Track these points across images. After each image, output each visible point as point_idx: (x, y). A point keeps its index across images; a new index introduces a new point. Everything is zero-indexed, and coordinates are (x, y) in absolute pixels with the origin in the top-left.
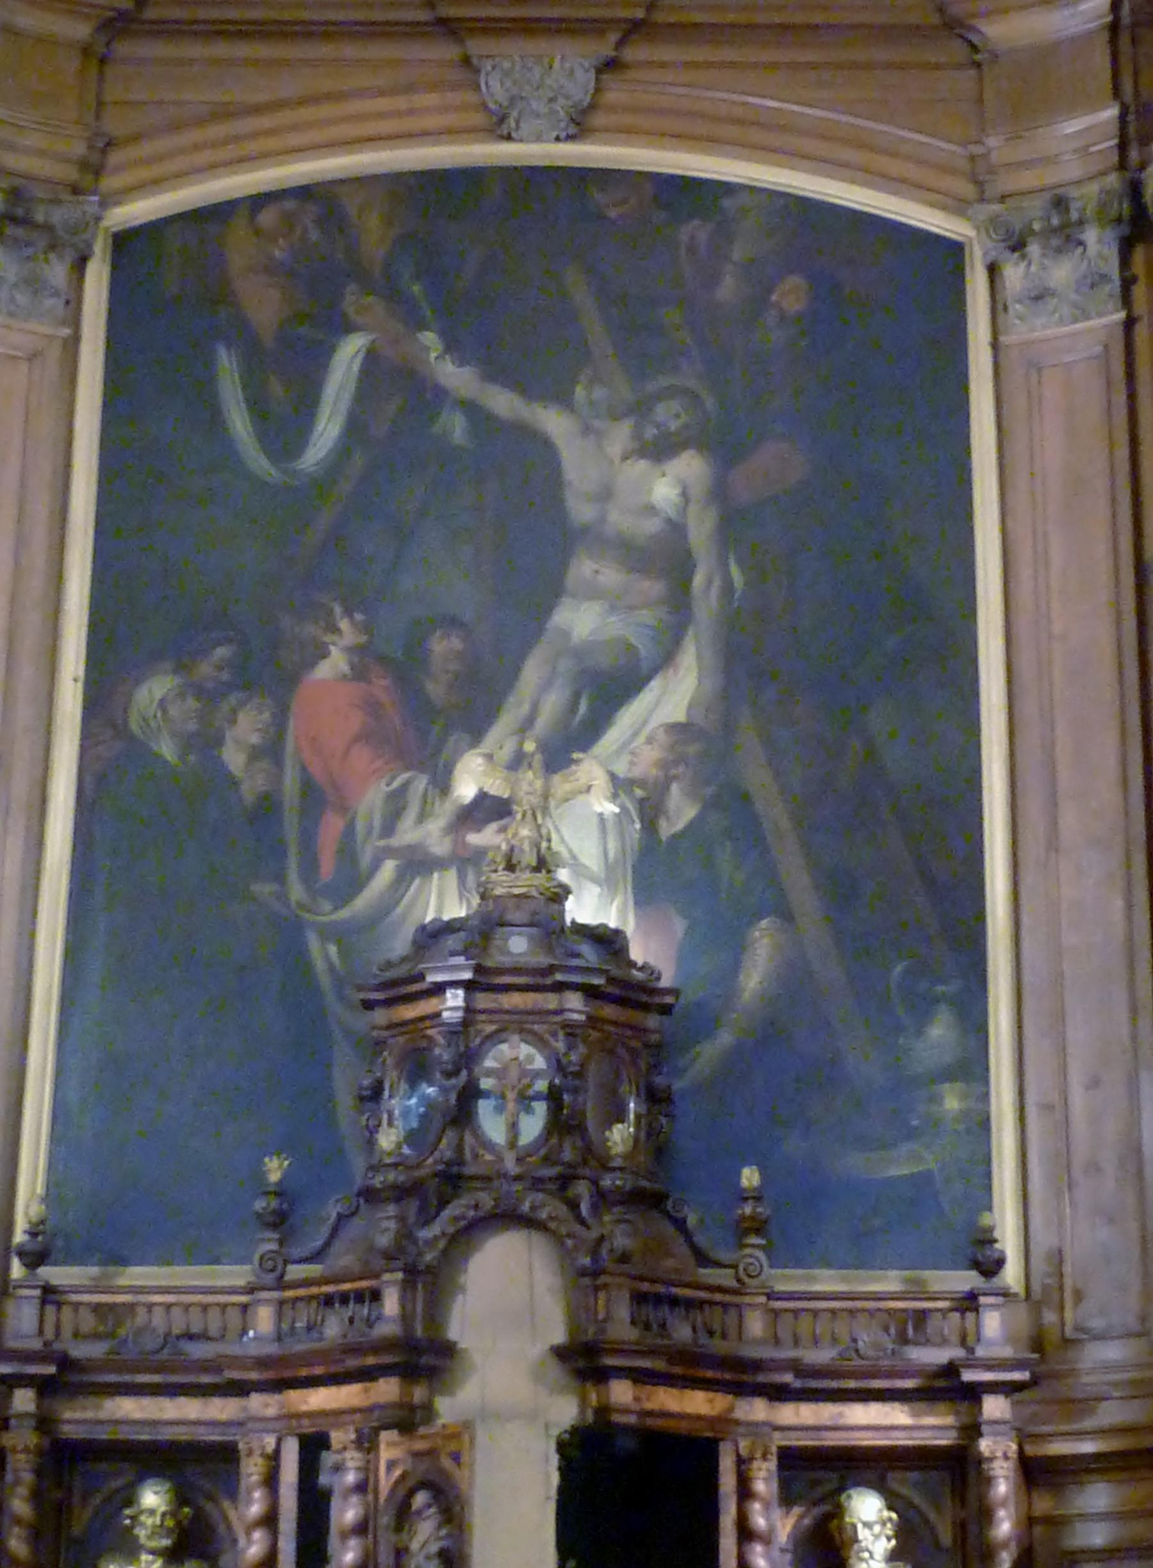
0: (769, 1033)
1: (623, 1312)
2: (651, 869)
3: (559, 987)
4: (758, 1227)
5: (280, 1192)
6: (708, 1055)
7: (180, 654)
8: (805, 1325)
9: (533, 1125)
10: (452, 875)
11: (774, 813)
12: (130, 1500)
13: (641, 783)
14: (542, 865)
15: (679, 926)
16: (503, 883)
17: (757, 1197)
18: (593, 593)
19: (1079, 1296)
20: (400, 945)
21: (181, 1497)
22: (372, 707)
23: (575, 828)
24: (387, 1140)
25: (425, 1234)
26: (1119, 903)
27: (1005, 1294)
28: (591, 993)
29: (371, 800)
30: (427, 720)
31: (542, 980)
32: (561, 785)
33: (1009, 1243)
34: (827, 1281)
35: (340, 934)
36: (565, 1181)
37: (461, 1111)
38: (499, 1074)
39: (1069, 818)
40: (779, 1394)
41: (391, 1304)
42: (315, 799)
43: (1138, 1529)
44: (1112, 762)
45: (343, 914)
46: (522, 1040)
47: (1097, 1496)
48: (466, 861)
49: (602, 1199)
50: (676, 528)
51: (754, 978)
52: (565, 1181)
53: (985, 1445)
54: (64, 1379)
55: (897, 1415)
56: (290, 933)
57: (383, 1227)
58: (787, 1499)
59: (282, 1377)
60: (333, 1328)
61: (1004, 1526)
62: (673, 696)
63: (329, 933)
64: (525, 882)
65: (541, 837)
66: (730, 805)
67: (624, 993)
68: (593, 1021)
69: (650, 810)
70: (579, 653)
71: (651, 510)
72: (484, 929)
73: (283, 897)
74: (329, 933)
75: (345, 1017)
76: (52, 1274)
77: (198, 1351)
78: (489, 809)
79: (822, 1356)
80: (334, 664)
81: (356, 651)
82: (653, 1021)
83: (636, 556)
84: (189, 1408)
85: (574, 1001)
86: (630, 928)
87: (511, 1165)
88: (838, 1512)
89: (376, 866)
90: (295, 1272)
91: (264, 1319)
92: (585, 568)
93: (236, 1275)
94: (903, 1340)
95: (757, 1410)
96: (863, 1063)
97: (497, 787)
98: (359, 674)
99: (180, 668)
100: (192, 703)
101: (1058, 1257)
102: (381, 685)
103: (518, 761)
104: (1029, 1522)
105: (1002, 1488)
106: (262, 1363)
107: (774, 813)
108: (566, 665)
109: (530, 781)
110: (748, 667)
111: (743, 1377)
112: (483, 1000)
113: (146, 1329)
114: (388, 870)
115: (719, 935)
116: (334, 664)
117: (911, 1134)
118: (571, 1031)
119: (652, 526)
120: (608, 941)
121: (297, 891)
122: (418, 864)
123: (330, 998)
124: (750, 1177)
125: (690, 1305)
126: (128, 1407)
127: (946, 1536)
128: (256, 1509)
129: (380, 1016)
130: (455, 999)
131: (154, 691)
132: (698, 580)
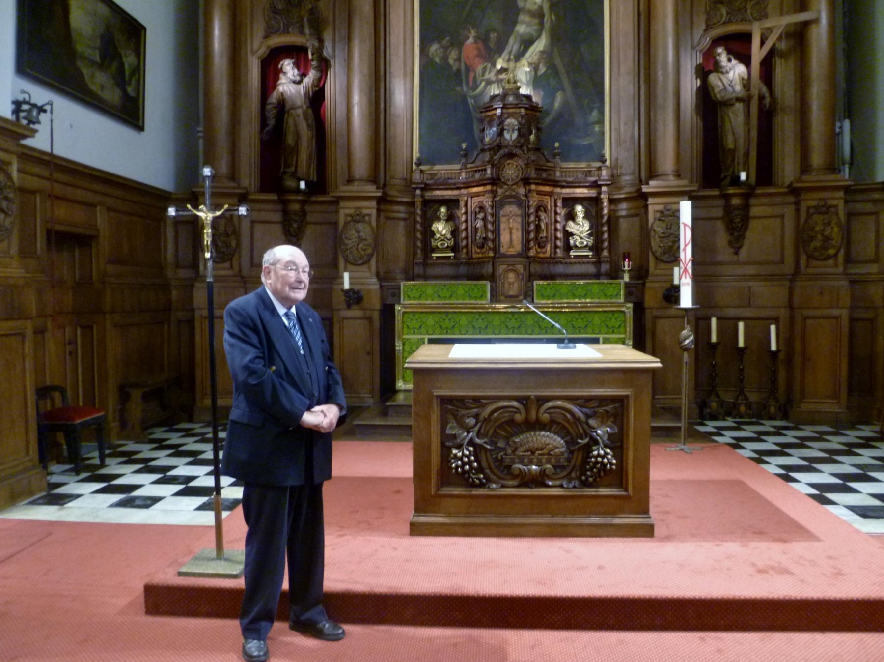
0: (560, 115)
1: (533, 171)
2: (537, 81)
3: (520, 108)
4: (559, 154)
5: (465, 150)
6: (548, 120)
7: (439, 38)
8: (567, 174)
9: (515, 135)
10: (496, 85)
11: (561, 69)
12: (439, 210)
13: (534, 63)
14: (515, 82)
15: (542, 93)
16: (507, 86)
17: (558, 148)
18: (523, 22)
19: (621, 167)
20: (487, 99)
21: (448, 210)
22: (478, 49)
23: (521, 74)
24: (487, 139)
25: (496, 157)
26: (632, 87)
27: (607, 167)
28: (526, 108)
29: (479, 69)
30: (490, 53)
31: (516, 106)
32: (518, 65)
33: (607, 156)
34: (571, 165)
35: (475, 97)
36: (521, 147)
37: (501, 133)
38: (508, 125)
39: (622, 69)
40: (563, 187)
41: (489, 171)
42: (468, 69)
43: (632, 212)
44: (631, 56)
45: (475, 93)
46: (329, 477)
47: (624, 206)
48: (499, 81)
49: (529, 150)
50: (541, 8)
51: (557, 104)
52: (521, 147)
53: (602, 196)
54: (426, 188)
55: (585, 191)
56: (464, 98)
57: (487, 156)
58: (564, 207)
59: (468, 186)
60: (477, 176)
61: (605, 211)
62: (540, 45)
63: (471, 97)
64: (512, 86)
65: (514, 76)
66: (552, 67)
67: (533, 108)
68: (526, 114)
69: (536, 69)
70: (521, 36)
71: (535, 4)
72: (504, 96)
73: (462, 90)
74: (471, 97)
75: (476, 115)
76: (423, 167)
77: (450, 181)
78: (503, 70)
79: (570, 179)
80: (471, 40)
81: (475, 37)
82: (538, 114)
83: (532, 14)
84: (449, 192)
85: (523, 110)
86: (532, 94)
87: (511, 143)
88: (573, 209)
89: (481, 83)
90: (469, 166)
91: (463, 175)
92: (522, 17)
93: (458, 166)
94: (586, 176)
95: (558, 190)
96: (579, 120)
97: (505, 66)
98: (476, 42)
99: (439, 42)
100: (442, 50)
101: (617, 159)
102: (481, 45)
103: (509, 60)
104: (610, 211)
105: (605, 204)
106: (464, 183)
107: (561, 69)
108: (518, 39)
109: (512, 64)
110: (555, 38)
111: (556, 184)
112: (505, 111)
113: (441, 178)
114: (483, 84)
115: (550, 96)
116: (471, 40)
117: (588, 135)
118: (522, 116)
119: (536, 7)
120: (528, 97)
121: (465, 89)
122: (489, 82)
123: (473, 111)
124: (557, 145)
125: (546, 170)
126: (438, 193)
127: (594, 214)
128: (463, 211)
129: (484, 114)
130: (499, 111)
131: (434, 48)
132: (546, 19)
